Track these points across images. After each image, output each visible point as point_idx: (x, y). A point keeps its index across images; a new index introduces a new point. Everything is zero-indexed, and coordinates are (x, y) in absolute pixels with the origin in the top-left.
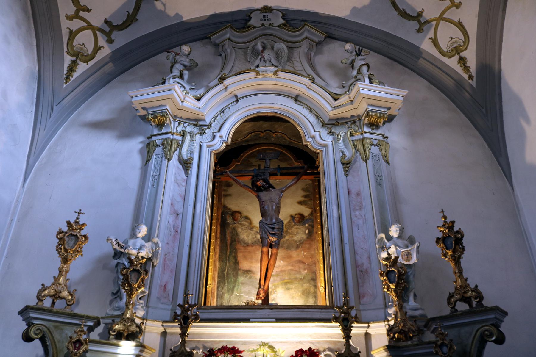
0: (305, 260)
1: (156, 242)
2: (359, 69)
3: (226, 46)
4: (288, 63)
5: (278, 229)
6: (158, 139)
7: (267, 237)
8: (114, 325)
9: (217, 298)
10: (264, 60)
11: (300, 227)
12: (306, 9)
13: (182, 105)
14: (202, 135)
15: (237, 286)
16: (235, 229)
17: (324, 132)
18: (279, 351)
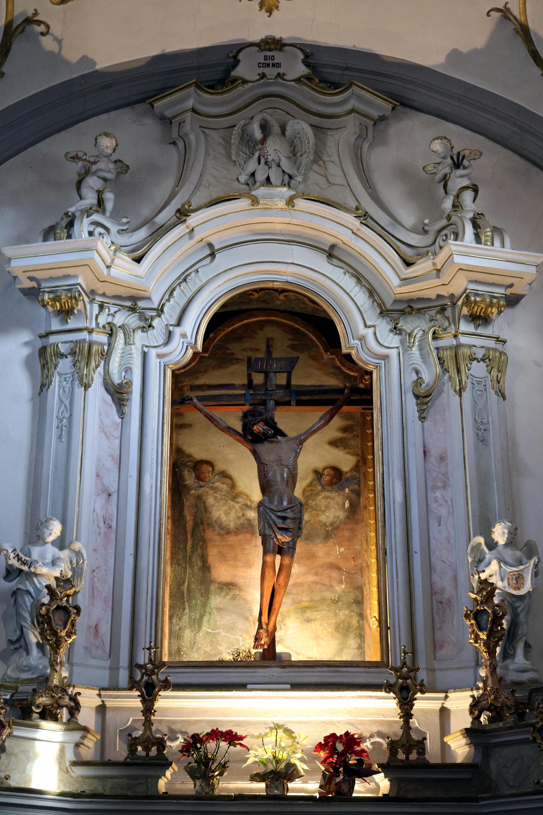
0: (341, 564)
1: (77, 550)
2: (458, 196)
3: (187, 127)
4: (315, 167)
5: (292, 519)
6: (63, 341)
7: (273, 535)
8: (37, 698)
9: (170, 639)
10: (266, 163)
11: (333, 495)
12: (354, 46)
13: (109, 274)
14: (146, 332)
15: (208, 614)
16: (201, 499)
18: (300, 737)
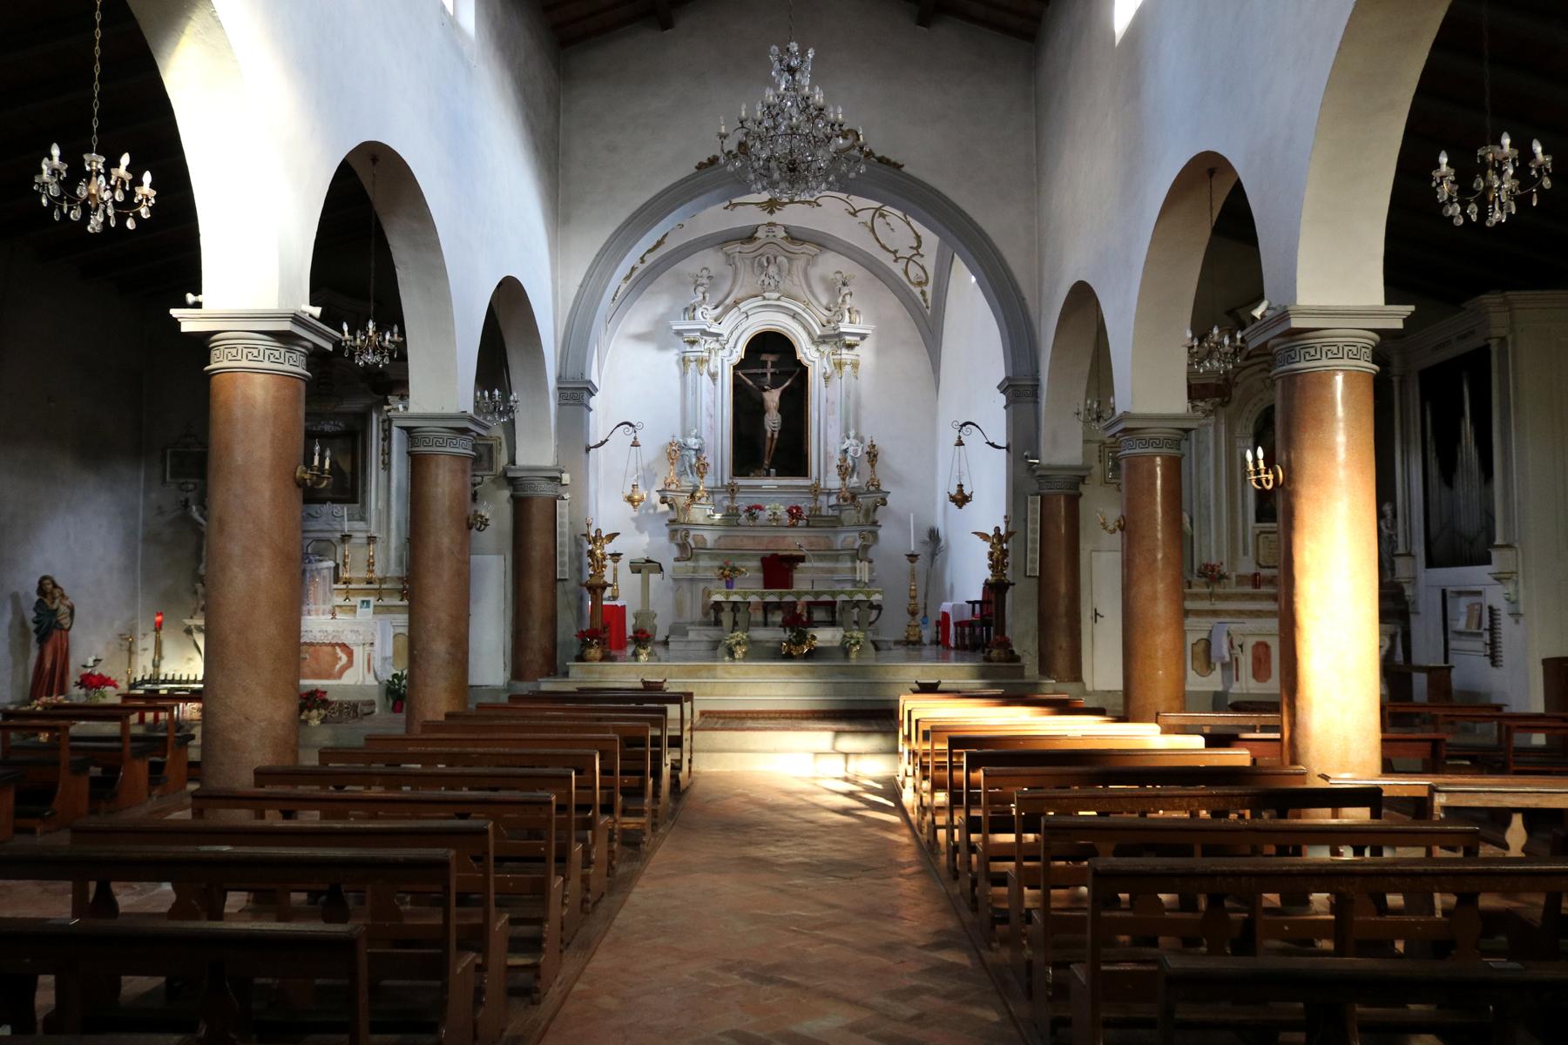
17: (813, 348)
